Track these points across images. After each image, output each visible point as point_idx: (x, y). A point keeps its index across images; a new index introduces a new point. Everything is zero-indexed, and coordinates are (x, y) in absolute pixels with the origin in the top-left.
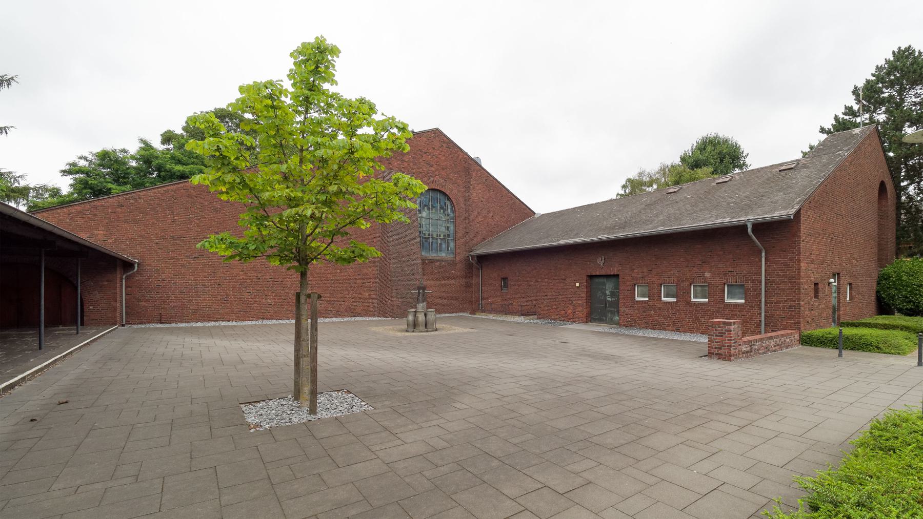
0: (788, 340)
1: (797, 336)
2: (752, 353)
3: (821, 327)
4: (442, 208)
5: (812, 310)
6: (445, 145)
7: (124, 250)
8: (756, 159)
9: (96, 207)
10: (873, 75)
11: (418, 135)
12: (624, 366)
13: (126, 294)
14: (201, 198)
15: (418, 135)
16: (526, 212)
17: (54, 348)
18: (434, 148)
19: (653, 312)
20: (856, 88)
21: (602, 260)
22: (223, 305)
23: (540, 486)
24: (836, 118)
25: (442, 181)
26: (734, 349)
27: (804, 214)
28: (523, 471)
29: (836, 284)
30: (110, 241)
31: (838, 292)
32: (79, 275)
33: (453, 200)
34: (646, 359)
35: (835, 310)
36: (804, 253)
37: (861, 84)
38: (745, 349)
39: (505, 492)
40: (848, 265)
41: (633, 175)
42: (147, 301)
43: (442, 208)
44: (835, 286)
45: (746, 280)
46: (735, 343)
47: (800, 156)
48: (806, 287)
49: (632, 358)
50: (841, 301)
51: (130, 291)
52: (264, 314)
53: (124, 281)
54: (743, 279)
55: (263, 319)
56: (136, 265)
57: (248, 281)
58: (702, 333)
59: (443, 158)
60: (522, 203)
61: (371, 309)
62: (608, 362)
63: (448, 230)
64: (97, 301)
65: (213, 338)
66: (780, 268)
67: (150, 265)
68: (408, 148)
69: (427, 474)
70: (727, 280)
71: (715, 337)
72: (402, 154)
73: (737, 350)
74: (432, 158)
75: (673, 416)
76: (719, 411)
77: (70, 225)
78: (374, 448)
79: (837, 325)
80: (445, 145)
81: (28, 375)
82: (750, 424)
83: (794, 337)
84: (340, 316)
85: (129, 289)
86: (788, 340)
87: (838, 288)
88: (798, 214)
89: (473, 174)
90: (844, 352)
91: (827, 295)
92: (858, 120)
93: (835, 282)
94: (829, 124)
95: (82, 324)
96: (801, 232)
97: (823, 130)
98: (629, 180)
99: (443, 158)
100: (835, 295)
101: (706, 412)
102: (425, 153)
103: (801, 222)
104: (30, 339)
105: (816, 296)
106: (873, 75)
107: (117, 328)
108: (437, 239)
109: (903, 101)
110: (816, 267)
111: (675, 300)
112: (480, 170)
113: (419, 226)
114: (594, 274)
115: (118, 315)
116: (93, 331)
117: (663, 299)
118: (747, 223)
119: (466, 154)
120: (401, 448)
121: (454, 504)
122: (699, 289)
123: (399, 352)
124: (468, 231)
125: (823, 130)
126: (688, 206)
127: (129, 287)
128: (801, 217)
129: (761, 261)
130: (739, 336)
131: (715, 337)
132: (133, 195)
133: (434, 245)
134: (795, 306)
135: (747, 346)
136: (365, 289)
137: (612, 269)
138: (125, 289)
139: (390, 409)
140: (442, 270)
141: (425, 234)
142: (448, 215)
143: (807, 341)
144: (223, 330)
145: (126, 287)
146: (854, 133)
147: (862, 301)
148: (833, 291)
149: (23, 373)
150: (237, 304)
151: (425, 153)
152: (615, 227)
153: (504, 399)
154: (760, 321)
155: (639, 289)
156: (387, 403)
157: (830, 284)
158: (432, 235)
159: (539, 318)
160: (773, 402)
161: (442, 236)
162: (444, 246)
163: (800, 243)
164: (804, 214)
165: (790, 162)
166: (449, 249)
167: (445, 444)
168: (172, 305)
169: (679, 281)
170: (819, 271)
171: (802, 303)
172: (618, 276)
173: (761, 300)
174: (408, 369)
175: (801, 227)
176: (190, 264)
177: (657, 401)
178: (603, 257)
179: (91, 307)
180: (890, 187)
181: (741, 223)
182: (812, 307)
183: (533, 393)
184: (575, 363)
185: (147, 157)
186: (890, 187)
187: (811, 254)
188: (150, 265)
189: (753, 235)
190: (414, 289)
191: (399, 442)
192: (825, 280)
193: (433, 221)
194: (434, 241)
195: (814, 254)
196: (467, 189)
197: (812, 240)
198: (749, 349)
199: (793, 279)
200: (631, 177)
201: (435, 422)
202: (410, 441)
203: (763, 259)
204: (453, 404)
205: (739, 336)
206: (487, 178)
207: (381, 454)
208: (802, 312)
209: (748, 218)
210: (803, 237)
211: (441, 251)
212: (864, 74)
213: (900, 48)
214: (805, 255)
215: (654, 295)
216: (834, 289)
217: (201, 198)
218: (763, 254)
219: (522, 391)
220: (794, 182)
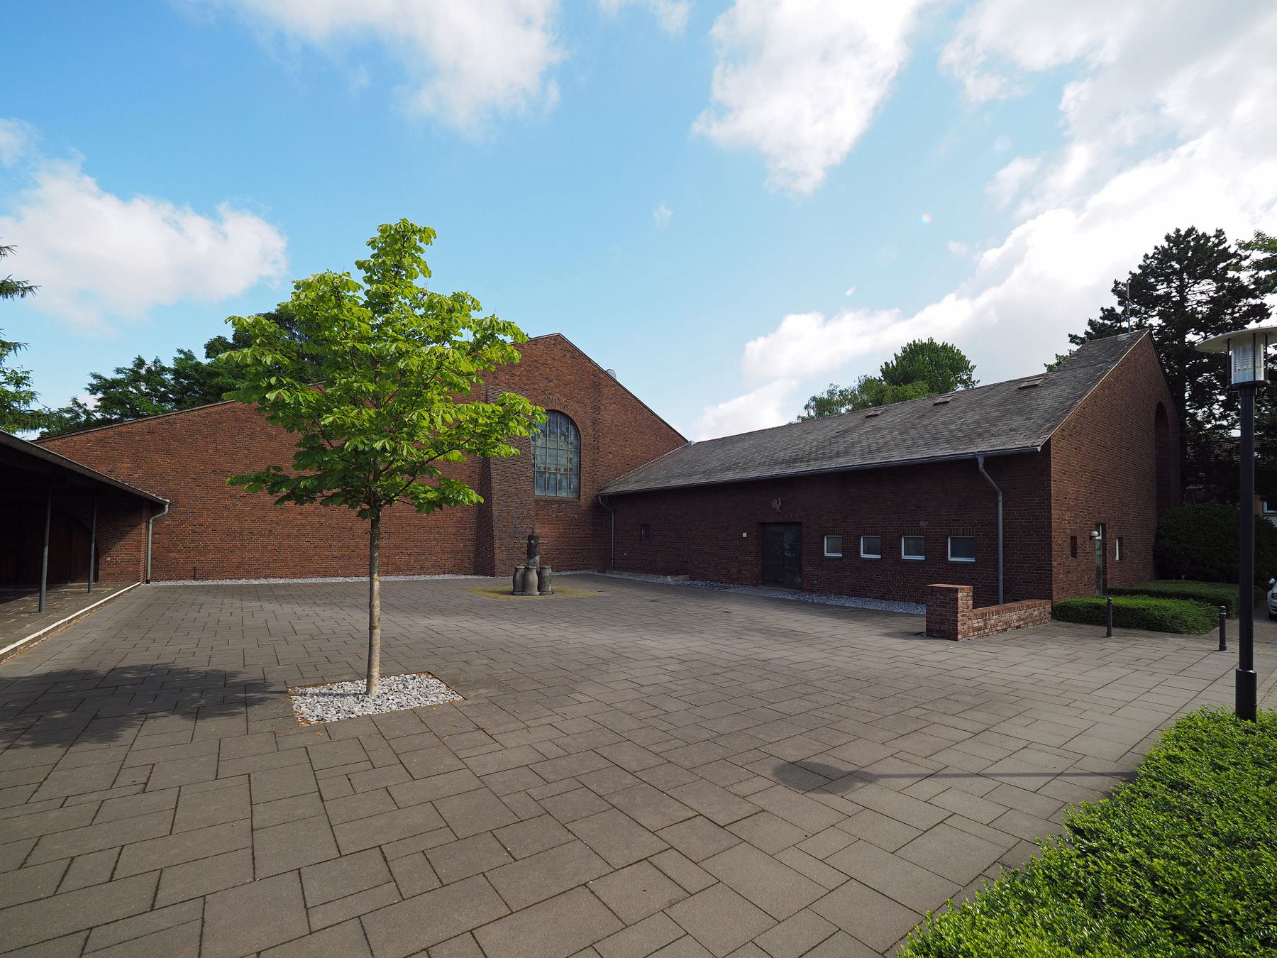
0: (1036, 613)
1: (1048, 607)
2: (986, 631)
3: (1080, 595)
4: (562, 434)
5: (1069, 572)
6: (568, 355)
7: (152, 487)
8: (987, 372)
9: (120, 434)
10: (1140, 267)
11: (534, 343)
12: (810, 646)
13: (153, 543)
14: (252, 422)
15: (534, 343)
16: (676, 439)
17: (58, 610)
18: (554, 359)
19: (848, 573)
20: (1193, 229)
21: (778, 503)
22: (274, 558)
23: (691, 814)
24: (1091, 323)
25: (563, 400)
26: (962, 625)
27: (1055, 446)
28: (668, 792)
29: (1100, 538)
30: (137, 476)
31: (1103, 549)
32: (95, 517)
33: (578, 424)
34: (840, 637)
35: (1102, 571)
36: (1056, 497)
37: (1124, 278)
38: (977, 625)
39: (642, 821)
40: (1117, 513)
41: (822, 393)
42: (178, 551)
43: (562, 434)
44: (1100, 540)
45: (976, 532)
46: (963, 616)
47: (1044, 370)
48: (1060, 542)
49: (819, 635)
50: (1108, 561)
51: (158, 538)
52: (327, 570)
53: (151, 526)
54: (973, 530)
55: (325, 576)
56: (167, 506)
57: (307, 527)
58: (918, 602)
59: (565, 370)
60: (680, 435)
61: (467, 565)
62: (787, 640)
63: (570, 463)
64: (116, 551)
65: (260, 600)
66: (1023, 516)
67: (183, 506)
68: (517, 355)
69: (534, 792)
70: (951, 532)
71: (935, 608)
72: (512, 365)
73: (966, 626)
74: (551, 370)
75: (879, 716)
76: (942, 711)
77: (87, 456)
78: (462, 754)
79: (1103, 592)
80: (568, 355)
81: (21, 645)
82: (987, 729)
83: (1045, 608)
84: (426, 573)
85: (157, 536)
86: (1036, 613)
87: (1104, 542)
88: (1047, 445)
89: (605, 390)
90: (1114, 630)
91: (1088, 553)
92: (1125, 325)
93: (1099, 535)
94: (1082, 330)
95: (96, 579)
96: (1052, 469)
97: (1073, 339)
98: (814, 399)
99: (565, 370)
100: (1099, 553)
101: (924, 711)
102: (542, 364)
103: (1052, 456)
104: (31, 601)
105: (1074, 554)
106: (1140, 267)
107: (140, 585)
108: (555, 474)
109: (1184, 299)
110: (1073, 515)
111: (879, 557)
112: (613, 386)
113: (532, 457)
114: (768, 521)
115: (141, 568)
116: (110, 589)
117: (863, 555)
118: (977, 456)
119: (596, 365)
120: (499, 755)
121: (570, 837)
122: (911, 542)
123: (503, 622)
124: (597, 463)
125: (1073, 339)
126: (896, 433)
127: (157, 534)
128: (1052, 449)
129: (997, 507)
130: (968, 607)
131: (935, 608)
132: (167, 418)
133: (552, 482)
134: (1045, 567)
135: (979, 620)
136: (459, 539)
137: (791, 515)
138: (152, 536)
139: (486, 701)
140: (562, 514)
141: (539, 468)
142: (571, 444)
143: (1064, 614)
144: (273, 590)
145: (154, 534)
146: (1120, 340)
147: (1136, 561)
148: (1097, 547)
149: (14, 642)
150: (292, 557)
151: (542, 364)
152: (795, 459)
153: (644, 690)
154: (997, 586)
155: (829, 542)
156: (482, 691)
157: (1092, 537)
158: (549, 469)
159: (692, 578)
160: (1019, 699)
161: (562, 469)
162: (564, 483)
163: (1050, 483)
164: (1055, 446)
165: (1033, 377)
166: (572, 486)
167: (560, 752)
168: (211, 556)
169: (885, 532)
170: (1078, 520)
171: (1055, 563)
172: (800, 523)
173: (998, 558)
174: (512, 645)
175: (1052, 463)
176: (235, 505)
177: (857, 695)
178: (780, 499)
179: (109, 559)
180: (1170, 410)
181: (969, 456)
182: (1068, 569)
183: (683, 682)
184: (741, 641)
185: (185, 366)
186: (1170, 410)
187: (1066, 498)
188: (183, 506)
189: (986, 473)
190: (523, 539)
191: (497, 746)
192: (1085, 533)
193: (551, 451)
194: (552, 476)
195: (1069, 498)
196: (597, 409)
197: (1065, 480)
198: (982, 624)
199: (1041, 532)
200: (818, 395)
201: (548, 720)
202: (512, 746)
203: (1000, 505)
204: (572, 696)
205: (968, 607)
206: (623, 396)
207: (470, 762)
208: (1054, 575)
209: (979, 450)
210: (1054, 476)
211: (560, 489)
212: (1128, 263)
213: (1178, 230)
214: (1057, 500)
215: (850, 550)
216: (1098, 545)
217: (252, 422)
218: (1000, 498)
219: (668, 678)
220: (1041, 403)
